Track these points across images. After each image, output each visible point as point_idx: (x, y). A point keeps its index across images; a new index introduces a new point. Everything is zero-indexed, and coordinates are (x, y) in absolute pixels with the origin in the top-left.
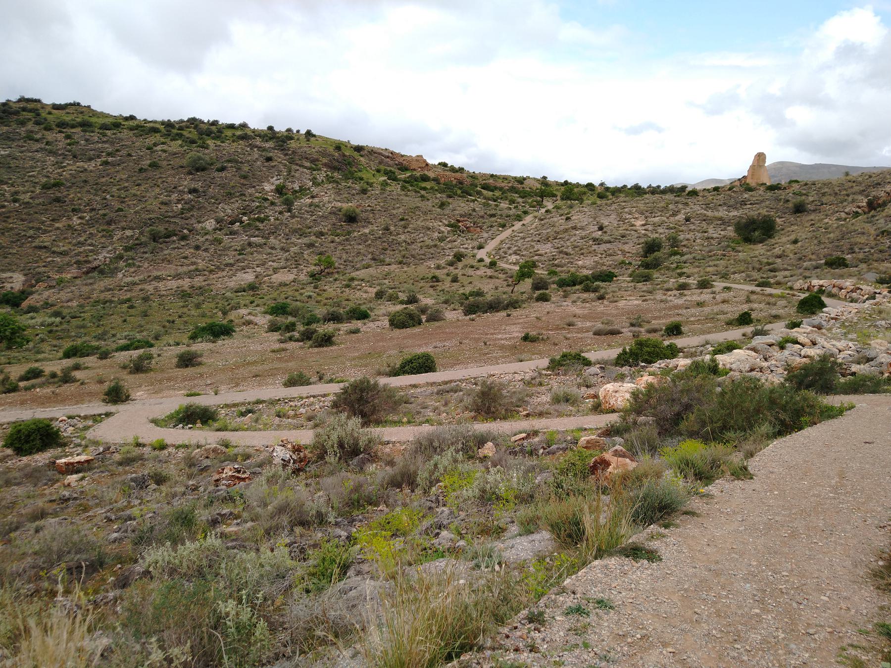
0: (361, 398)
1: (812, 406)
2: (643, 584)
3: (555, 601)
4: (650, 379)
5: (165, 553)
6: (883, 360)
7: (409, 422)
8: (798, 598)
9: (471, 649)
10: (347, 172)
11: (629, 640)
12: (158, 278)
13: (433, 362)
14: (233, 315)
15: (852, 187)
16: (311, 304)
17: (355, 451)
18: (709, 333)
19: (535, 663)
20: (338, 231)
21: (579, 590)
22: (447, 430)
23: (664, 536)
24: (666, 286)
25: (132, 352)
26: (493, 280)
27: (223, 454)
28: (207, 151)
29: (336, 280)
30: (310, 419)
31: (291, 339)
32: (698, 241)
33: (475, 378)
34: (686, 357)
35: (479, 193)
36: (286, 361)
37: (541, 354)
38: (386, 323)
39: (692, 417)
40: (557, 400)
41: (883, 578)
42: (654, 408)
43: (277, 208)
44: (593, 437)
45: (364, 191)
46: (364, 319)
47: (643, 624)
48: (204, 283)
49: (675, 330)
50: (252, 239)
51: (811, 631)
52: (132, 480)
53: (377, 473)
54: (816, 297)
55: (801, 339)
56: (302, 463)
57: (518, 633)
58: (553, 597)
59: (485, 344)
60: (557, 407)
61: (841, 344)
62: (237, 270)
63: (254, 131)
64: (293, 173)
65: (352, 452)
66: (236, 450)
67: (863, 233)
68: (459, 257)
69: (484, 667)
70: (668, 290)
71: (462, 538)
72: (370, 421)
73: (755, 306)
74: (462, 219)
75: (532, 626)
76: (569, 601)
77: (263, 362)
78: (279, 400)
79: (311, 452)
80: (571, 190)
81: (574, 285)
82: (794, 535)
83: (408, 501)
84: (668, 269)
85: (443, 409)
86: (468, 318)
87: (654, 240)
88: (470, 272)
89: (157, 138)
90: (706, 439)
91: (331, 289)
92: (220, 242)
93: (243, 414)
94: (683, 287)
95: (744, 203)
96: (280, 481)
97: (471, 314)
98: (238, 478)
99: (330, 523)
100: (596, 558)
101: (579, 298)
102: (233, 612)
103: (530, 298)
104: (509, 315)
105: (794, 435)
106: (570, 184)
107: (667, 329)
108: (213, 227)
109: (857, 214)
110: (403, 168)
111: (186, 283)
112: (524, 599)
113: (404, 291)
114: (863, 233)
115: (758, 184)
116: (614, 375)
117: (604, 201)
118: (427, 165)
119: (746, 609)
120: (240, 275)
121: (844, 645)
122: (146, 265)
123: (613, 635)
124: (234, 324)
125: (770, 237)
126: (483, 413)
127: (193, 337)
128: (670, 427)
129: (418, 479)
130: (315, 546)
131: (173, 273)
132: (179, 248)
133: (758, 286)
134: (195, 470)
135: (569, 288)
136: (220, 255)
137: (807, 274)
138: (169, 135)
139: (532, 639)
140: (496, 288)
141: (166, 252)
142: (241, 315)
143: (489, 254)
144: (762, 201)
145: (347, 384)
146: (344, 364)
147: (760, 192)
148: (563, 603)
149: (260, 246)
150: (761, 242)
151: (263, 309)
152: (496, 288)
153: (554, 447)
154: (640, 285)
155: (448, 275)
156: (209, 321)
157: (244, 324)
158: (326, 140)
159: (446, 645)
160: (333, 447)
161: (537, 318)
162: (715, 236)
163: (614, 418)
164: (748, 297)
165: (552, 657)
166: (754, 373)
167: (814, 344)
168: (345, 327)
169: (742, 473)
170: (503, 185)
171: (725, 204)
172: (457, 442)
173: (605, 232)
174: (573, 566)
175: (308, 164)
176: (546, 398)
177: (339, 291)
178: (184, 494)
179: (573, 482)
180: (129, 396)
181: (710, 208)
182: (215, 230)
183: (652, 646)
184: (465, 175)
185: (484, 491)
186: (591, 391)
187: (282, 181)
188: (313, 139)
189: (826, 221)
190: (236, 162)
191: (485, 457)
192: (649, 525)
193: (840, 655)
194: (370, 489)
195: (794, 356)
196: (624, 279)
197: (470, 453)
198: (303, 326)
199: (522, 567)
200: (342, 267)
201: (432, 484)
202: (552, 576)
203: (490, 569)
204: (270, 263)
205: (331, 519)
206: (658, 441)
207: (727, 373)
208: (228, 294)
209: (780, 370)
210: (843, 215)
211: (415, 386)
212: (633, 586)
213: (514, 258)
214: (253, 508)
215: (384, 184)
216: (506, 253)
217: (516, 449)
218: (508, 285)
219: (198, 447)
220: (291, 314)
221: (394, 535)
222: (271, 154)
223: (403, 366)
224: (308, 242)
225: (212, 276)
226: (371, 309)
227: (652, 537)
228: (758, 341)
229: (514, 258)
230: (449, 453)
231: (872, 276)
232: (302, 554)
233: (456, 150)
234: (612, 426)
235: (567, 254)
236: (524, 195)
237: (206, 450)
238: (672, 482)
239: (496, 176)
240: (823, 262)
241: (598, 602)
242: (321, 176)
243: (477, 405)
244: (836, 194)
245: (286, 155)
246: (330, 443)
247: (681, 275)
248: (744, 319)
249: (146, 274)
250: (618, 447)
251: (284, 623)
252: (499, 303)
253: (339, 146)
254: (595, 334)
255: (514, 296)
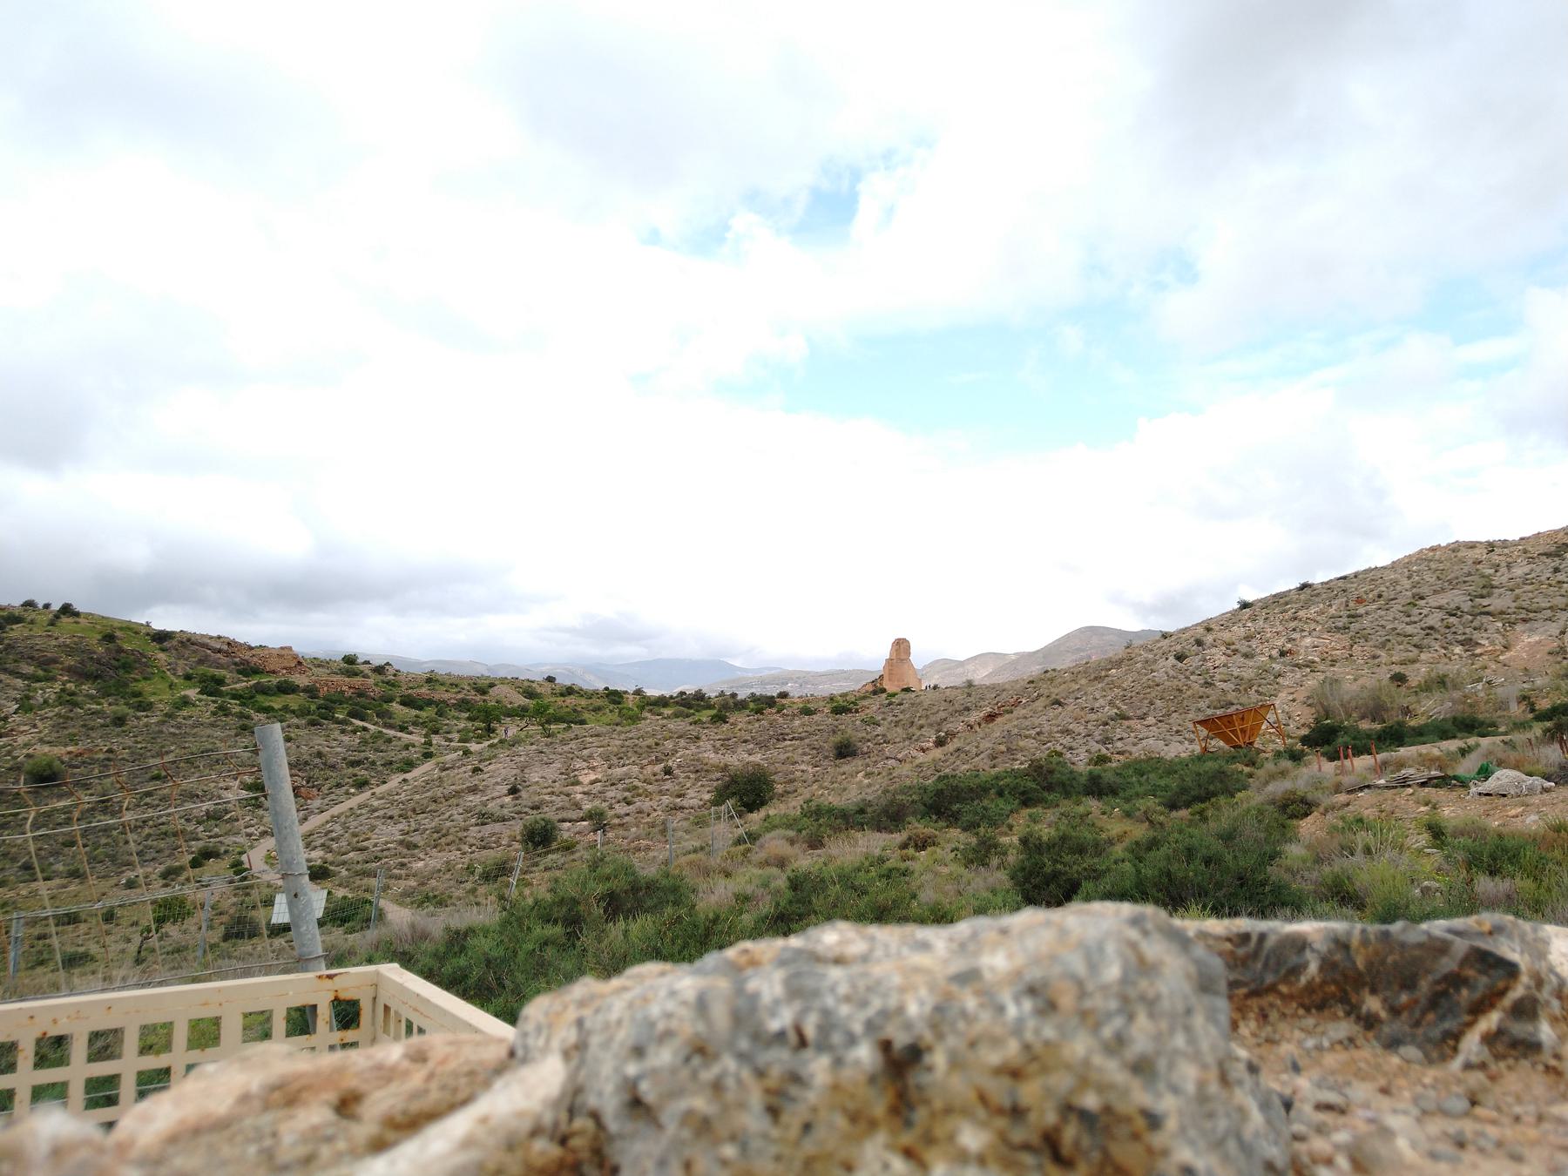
110: (247, 670)
170: (446, 696)
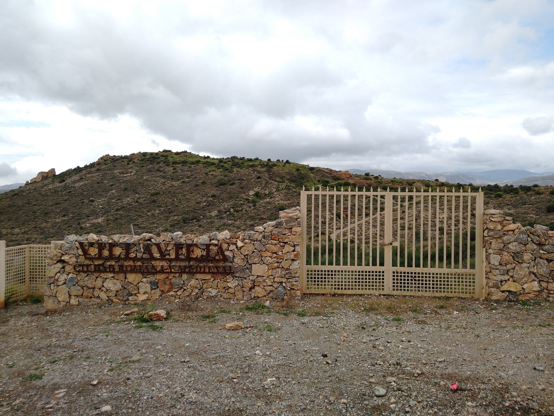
89: (213, 168)
175: (278, 179)
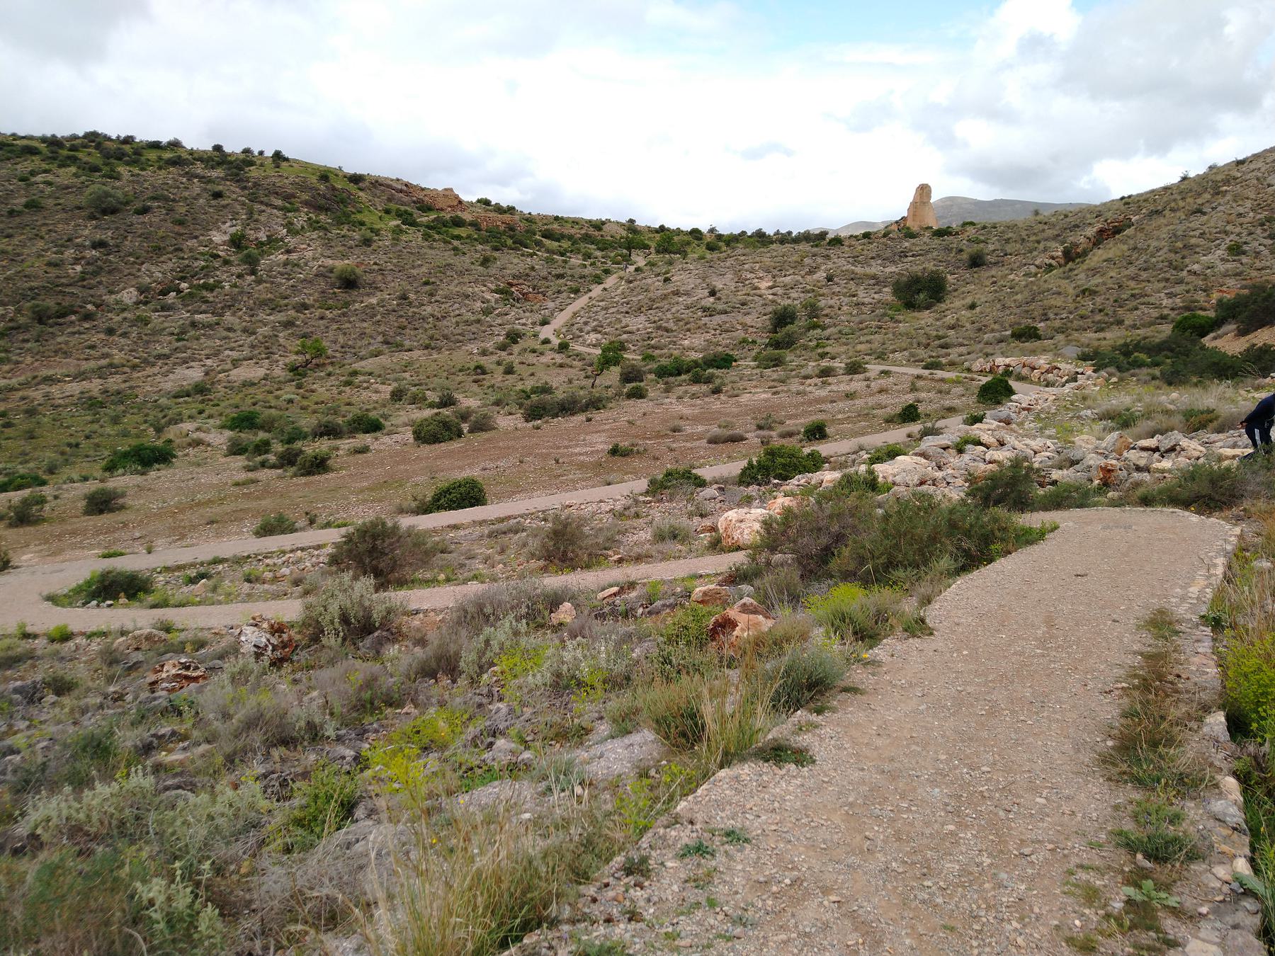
0: (374, 548)
1: (1005, 529)
2: (790, 800)
3: (664, 838)
4: (787, 501)
5: (63, 805)
6: (1091, 462)
7: (448, 580)
8: (1006, 803)
9: (539, 925)
10: (339, 214)
11: (775, 889)
12: (49, 380)
13: (481, 490)
14: (172, 432)
15: (1044, 230)
16: (294, 411)
17: (366, 628)
18: (863, 435)
19: (637, 940)
20: (330, 302)
21: (699, 817)
22: (503, 589)
23: (816, 727)
24: (803, 372)
25: (12, 494)
26: (565, 370)
27: (163, 642)
28: (118, 184)
29: (329, 375)
30: (297, 583)
31: (263, 465)
32: (845, 308)
33: (544, 512)
34: (833, 469)
35: (538, 243)
36: (258, 498)
37: (637, 474)
38: (409, 436)
39: (846, 552)
40: (660, 537)
41: (1115, 765)
42: (794, 542)
43: (234, 269)
44: (712, 586)
45: (367, 242)
46: (375, 431)
47: (793, 862)
48: (123, 386)
49: (817, 432)
50: (197, 317)
51: (1027, 851)
52: (16, 691)
53: (400, 657)
54: (1001, 381)
55: (985, 438)
56: (285, 650)
57: (611, 894)
58: (661, 831)
59: (557, 462)
60: (660, 546)
61: (1036, 443)
62: (175, 364)
63: (191, 152)
64: (256, 216)
65: (362, 629)
66: (182, 636)
67: (1059, 293)
68: (514, 337)
69: (560, 952)
70: (806, 377)
71: (527, 748)
72: (389, 582)
73: (923, 395)
74: (515, 282)
75: (631, 880)
76: (685, 836)
77: (222, 500)
78: (249, 557)
79: (299, 633)
80: (670, 239)
81: (679, 374)
82: (993, 712)
83: (446, 697)
84: (806, 348)
85: (498, 558)
86: (530, 425)
87: (785, 308)
88: (531, 358)
90: (866, 582)
91: (323, 388)
92: (146, 322)
93: (193, 581)
94: (826, 373)
95: (904, 254)
96: (252, 678)
97: (535, 419)
98: (186, 677)
99: (328, 737)
100: (721, 767)
101: (686, 392)
102: (162, 898)
103: (619, 394)
104: (589, 420)
105: (982, 569)
106: (668, 230)
107: (806, 432)
108: (134, 299)
109: (1050, 268)
110: (426, 208)
111: (95, 386)
112: (619, 835)
113: (434, 389)
114: (1059, 293)
115: (922, 228)
116: (738, 499)
117: (716, 255)
118: (460, 202)
119: (936, 826)
120: (181, 371)
121: (1072, 866)
122: (29, 359)
123: (751, 883)
124: (174, 445)
125: (940, 300)
126: (556, 561)
127: (110, 468)
128: (817, 566)
129: (462, 664)
130: (305, 775)
131: (73, 370)
132: (80, 333)
133: (926, 368)
134: (118, 669)
135: (672, 379)
136: (148, 342)
137: (989, 350)
138: (55, 159)
139: (632, 901)
140: (570, 381)
141: (59, 339)
142: (184, 432)
143: (557, 333)
144: (928, 252)
145: (351, 529)
146: (347, 499)
147: (925, 239)
148: (677, 839)
149: (210, 326)
150: (927, 308)
151: (218, 422)
152: (570, 381)
153: (658, 603)
154: (768, 372)
155: (499, 363)
156: (134, 442)
157: (190, 445)
158: (305, 166)
159: (499, 926)
160: (332, 622)
161: (629, 422)
162: (866, 300)
163: (739, 558)
164: (913, 384)
165: (662, 926)
166: (925, 487)
167: (1002, 444)
168: (346, 444)
169: (918, 628)
170: (572, 231)
171: (878, 256)
172: (518, 606)
173: (719, 299)
174: (689, 780)
175: (279, 202)
176: (646, 535)
177: (335, 390)
178: (101, 707)
179: (686, 654)
180: (8, 562)
181: (859, 262)
182: (137, 303)
183: (807, 895)
184: (517, 217)
185: (558, 675)
186: (707, 522)
187: (239, 228)
188: (284, 164)
189: (1011, 277)
190: (166, 199)
191: (561, 624)
192: (795, 711)
193: (1068, 883)
194: (389, 683)
195: (977, 462)
196: (746, 364)
197: (539, 620)
198: (281, 445)
199: (615, 786)
200: (338, 355)
201: (482, 669)
202: (658, 794)
203: (567, 793)
204: (227, 352)
205: (330, 732)
206: (800, 588)
207: (889, 489)
208: (163, 401)
209: (960, 482)
210: (1033, 269)
211: (455, 527)
212: (776, 804)
213: (593, 337)
214: (208, 723)
215: (397, 231)
216: (581, 331)
217: (606, 610)
218: (587, 377)
219: (123, 633)
220: (262, 428)
221: (426, 749)
222: (221, 188)
223: (436, 499)
224: (284, 319)
225: (136, 375)
226: (386, 417)
227: (800, 729)
228: (929, 443)
229: (593, 337)
230: (507, 623)
231: (1072, 351)
232: (283, 791)
233: (503, 181)
234: (737, 570)
235: (667, 330)
236: (604, 246)
237: (135, 638)
238: (824, 646)
239: (562, 218)
240: (1009, 333)
241: (728, 835)
242: (300, 220)
243: (548, 550)
244: (1023, 240)
245: (245, 188)
246: (328, 618)
247: (823, 356)
248: (909, 414)
249: (29, 374)
250: (746, 600)
251: (251, 901)
252: (575, 402)
253: (325, 175)
254: (710, 442)
255: (596, 393)
